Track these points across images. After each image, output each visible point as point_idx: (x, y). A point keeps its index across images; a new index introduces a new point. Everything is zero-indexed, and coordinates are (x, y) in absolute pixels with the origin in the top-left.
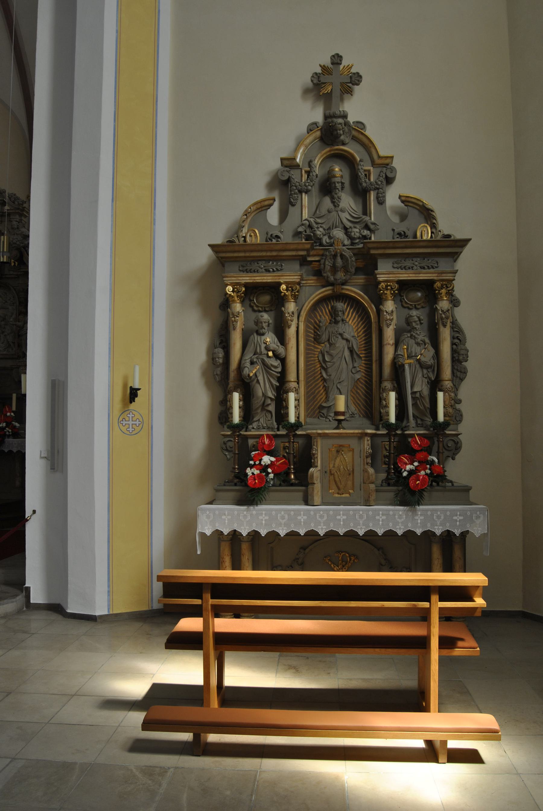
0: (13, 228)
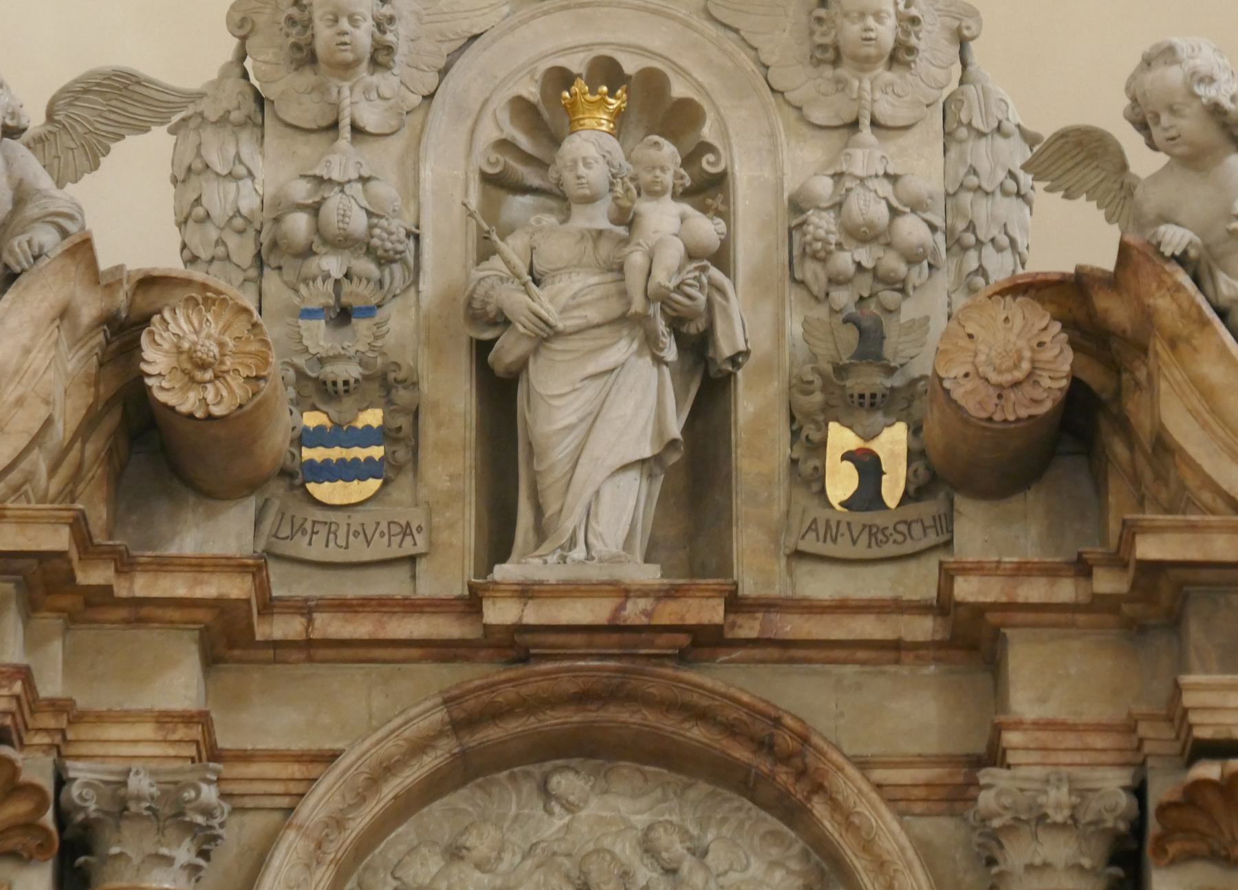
0: (832, 55)
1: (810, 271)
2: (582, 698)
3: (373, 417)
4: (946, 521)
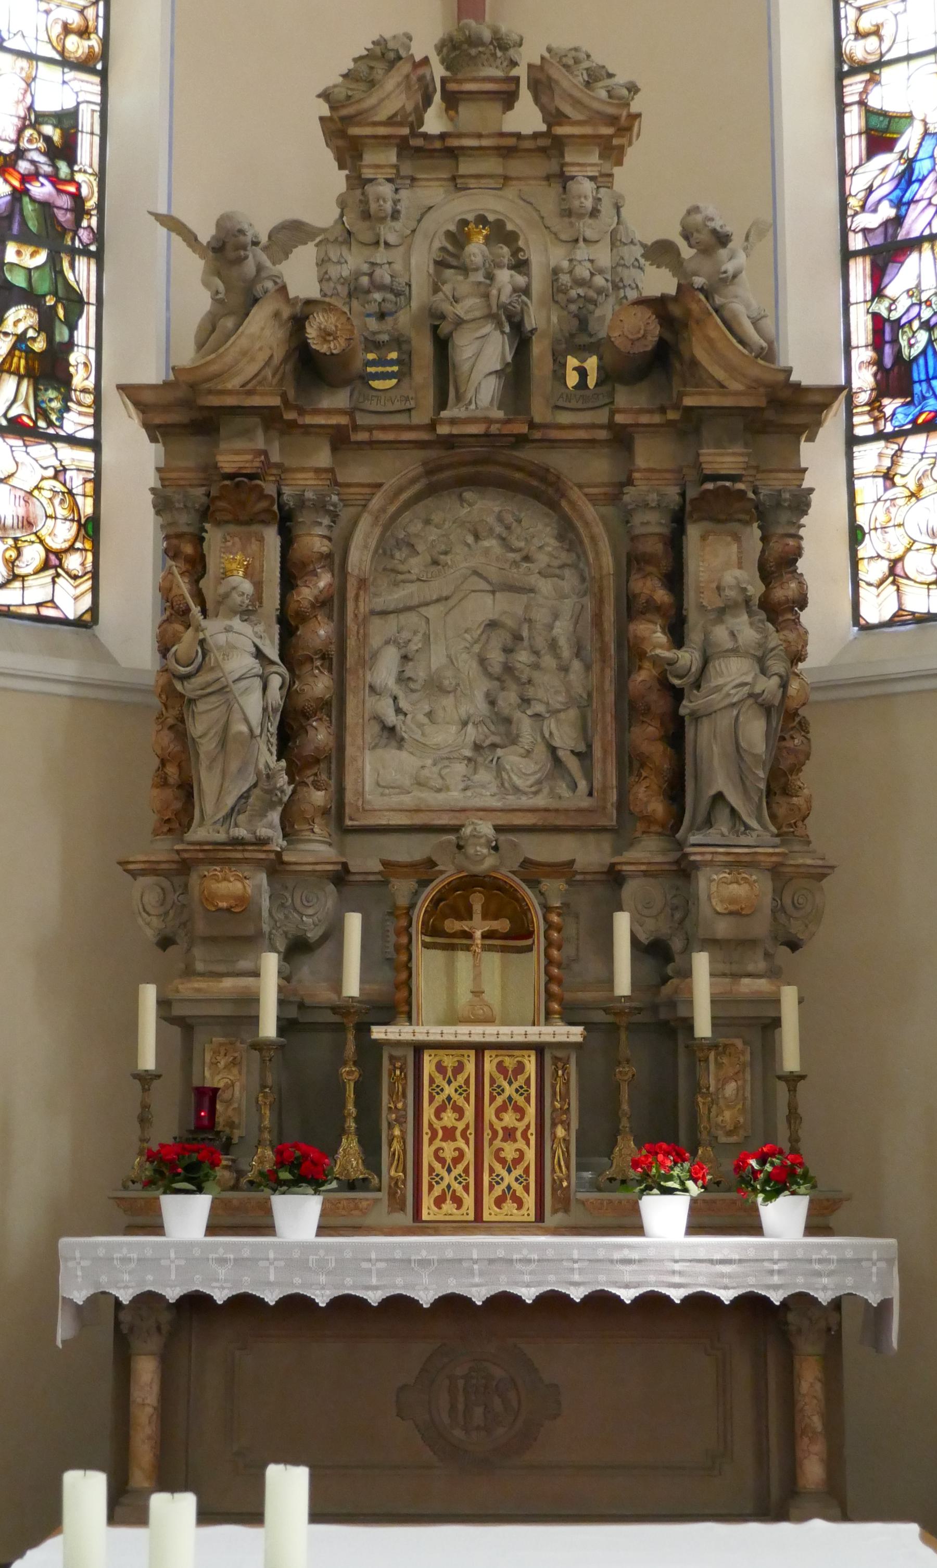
0: (568, 213)
1: (560, 297)
3: (394, 355)
4: (612, 394)
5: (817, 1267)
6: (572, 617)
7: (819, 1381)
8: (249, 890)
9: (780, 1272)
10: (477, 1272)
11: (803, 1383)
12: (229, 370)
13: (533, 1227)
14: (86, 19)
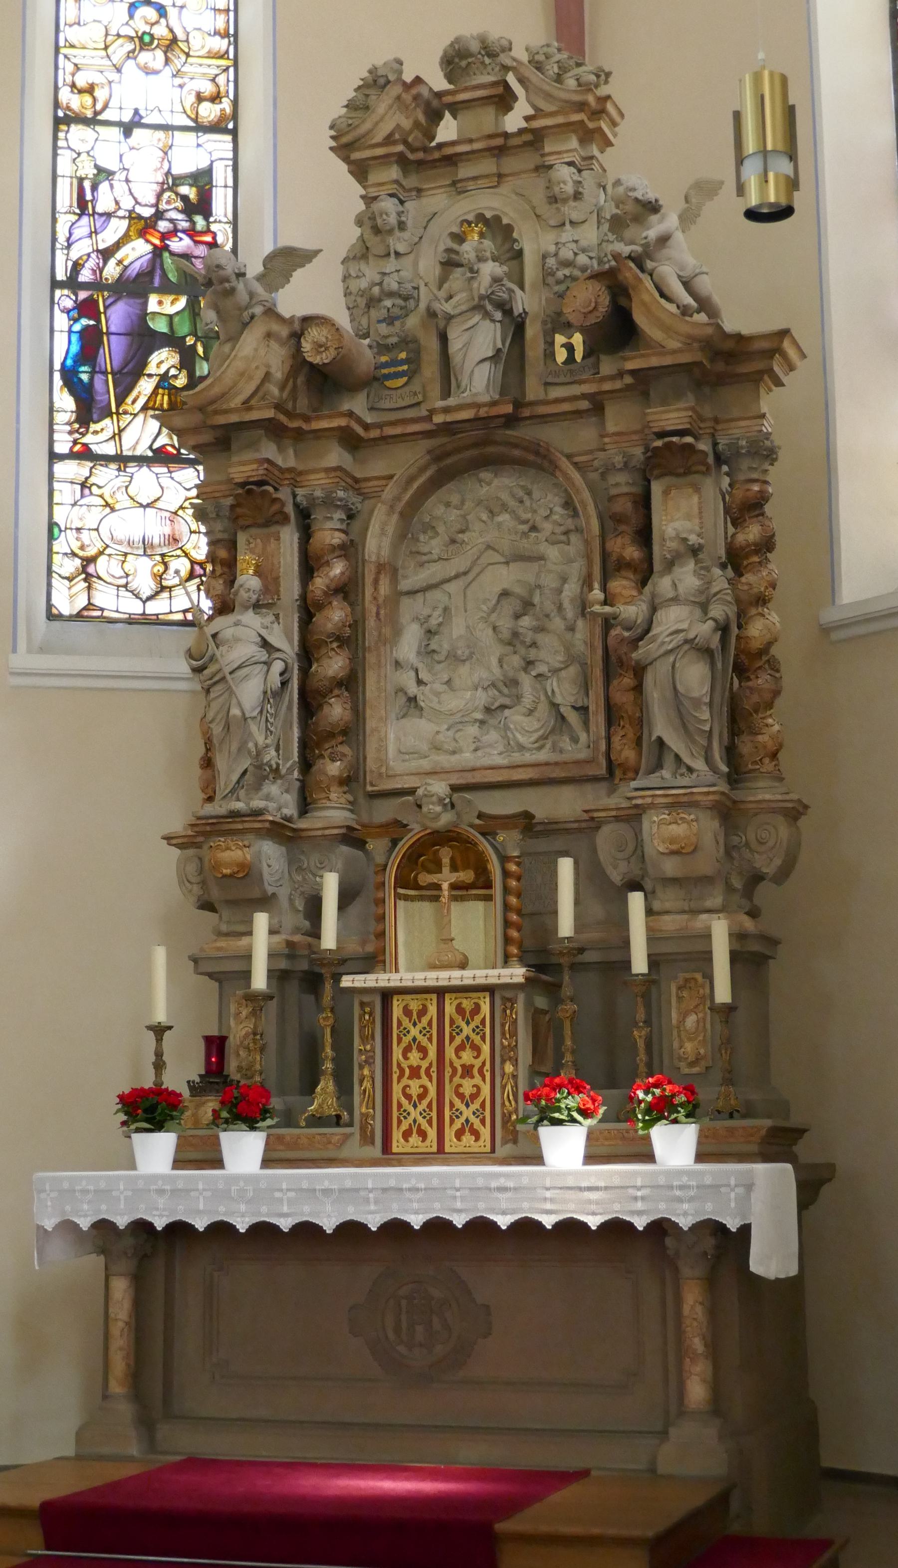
0: (553, 200)
1: (550, 280)
2: (476, 445)
3: (403, 355)
4: (596, 366)
5: (678, 1193)
6: (579, 580)
7: (700, 1303)
8: (248, 857)
9: (643, 1198)
10: (372, 1200)
11: (685, 1306)
12: (230, 390)
13: (487, 1158)
14: (217, 86)
